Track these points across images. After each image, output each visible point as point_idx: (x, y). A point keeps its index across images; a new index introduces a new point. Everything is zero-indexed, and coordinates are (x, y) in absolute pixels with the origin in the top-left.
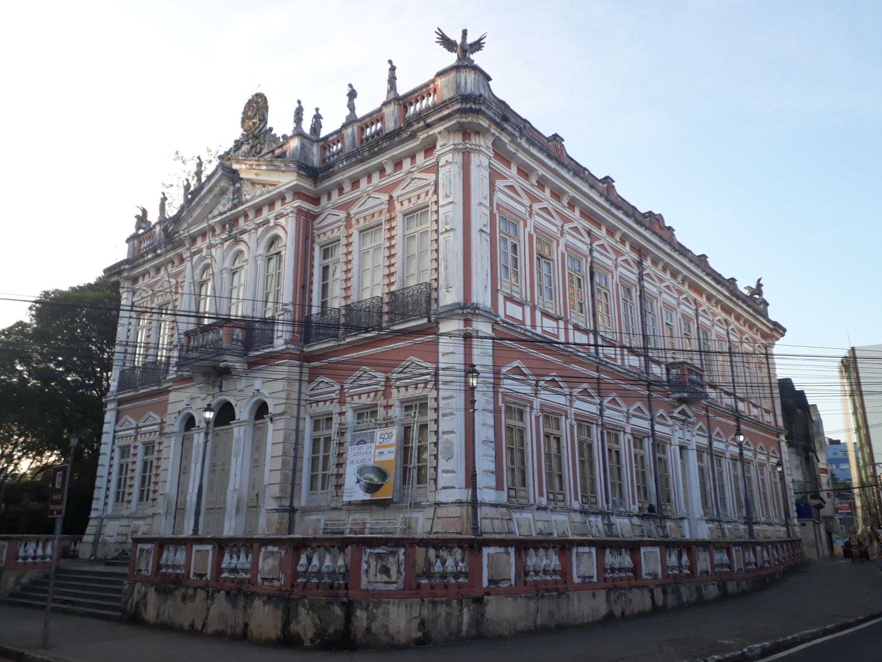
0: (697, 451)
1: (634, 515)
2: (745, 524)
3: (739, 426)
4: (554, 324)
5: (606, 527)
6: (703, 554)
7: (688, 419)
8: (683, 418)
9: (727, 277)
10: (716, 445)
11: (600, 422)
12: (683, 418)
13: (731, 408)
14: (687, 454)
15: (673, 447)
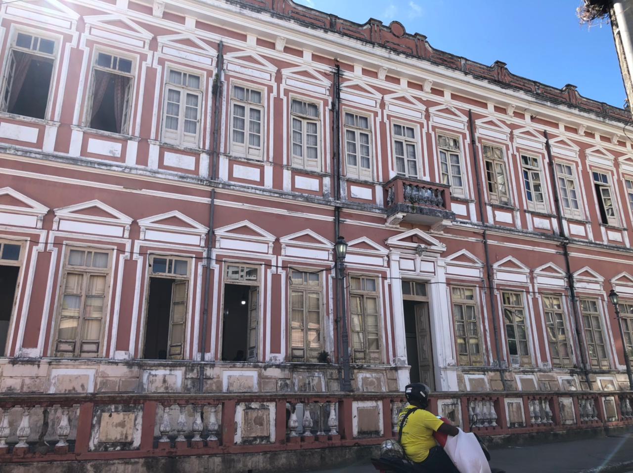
0: (448, 284)
1: (271, 366)
2: (572, 373)
3: (485, 243)
4: (582, 228)
5: (189, 382)
6: (118, 417)
7: (429, 247)
8: (415, 245)
9: (561, 86)
10: (501, 277)
11: (205, 255)
12: (415, 245)
13: (550, 233)
14: (431, 287)
15: (387, 282)
